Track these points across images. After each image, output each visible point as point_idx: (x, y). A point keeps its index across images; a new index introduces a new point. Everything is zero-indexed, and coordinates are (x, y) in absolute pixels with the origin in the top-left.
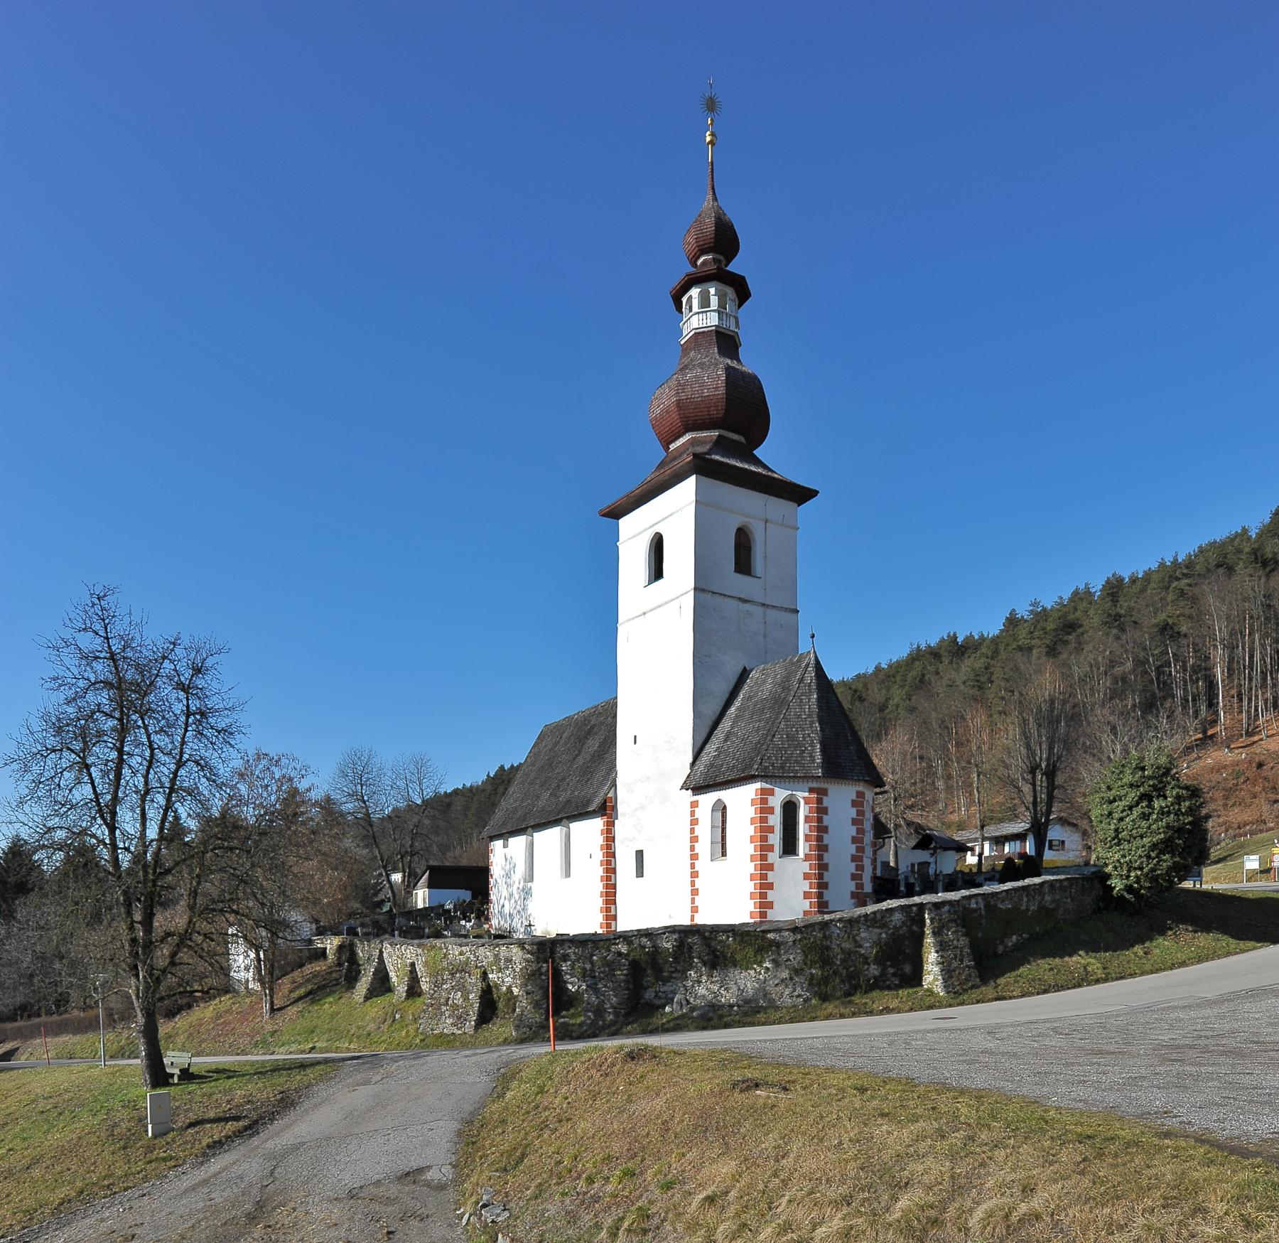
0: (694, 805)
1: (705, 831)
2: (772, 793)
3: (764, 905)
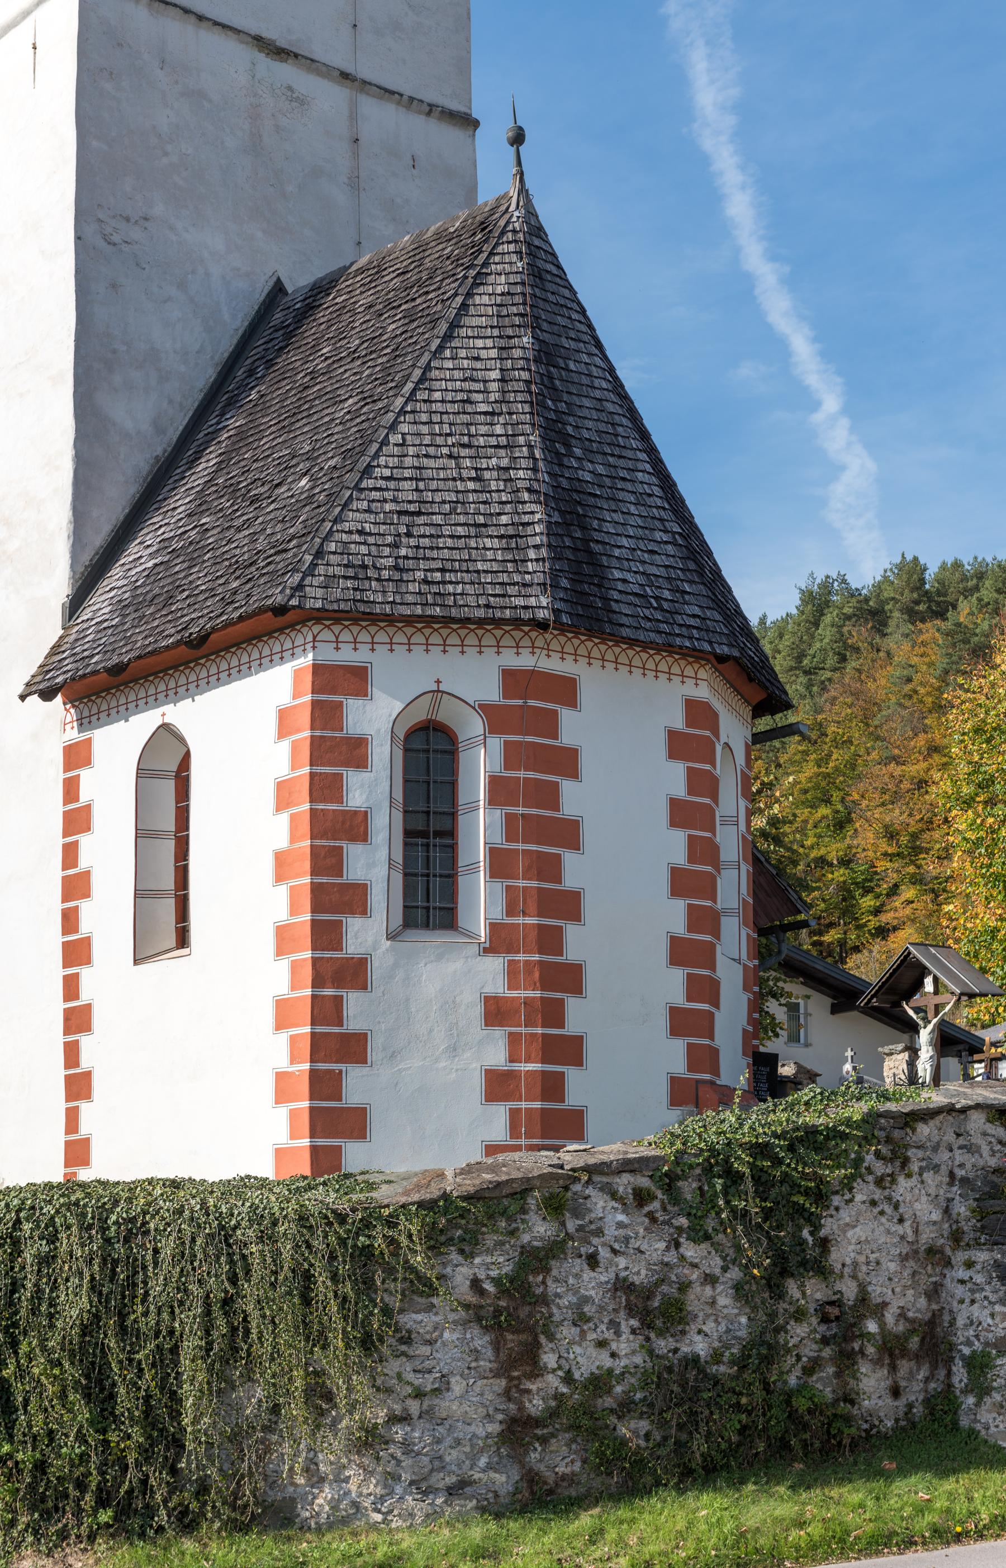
0: (77, 756)
1: (111, 852)
2: (357, 680)
3: (332, 1118)
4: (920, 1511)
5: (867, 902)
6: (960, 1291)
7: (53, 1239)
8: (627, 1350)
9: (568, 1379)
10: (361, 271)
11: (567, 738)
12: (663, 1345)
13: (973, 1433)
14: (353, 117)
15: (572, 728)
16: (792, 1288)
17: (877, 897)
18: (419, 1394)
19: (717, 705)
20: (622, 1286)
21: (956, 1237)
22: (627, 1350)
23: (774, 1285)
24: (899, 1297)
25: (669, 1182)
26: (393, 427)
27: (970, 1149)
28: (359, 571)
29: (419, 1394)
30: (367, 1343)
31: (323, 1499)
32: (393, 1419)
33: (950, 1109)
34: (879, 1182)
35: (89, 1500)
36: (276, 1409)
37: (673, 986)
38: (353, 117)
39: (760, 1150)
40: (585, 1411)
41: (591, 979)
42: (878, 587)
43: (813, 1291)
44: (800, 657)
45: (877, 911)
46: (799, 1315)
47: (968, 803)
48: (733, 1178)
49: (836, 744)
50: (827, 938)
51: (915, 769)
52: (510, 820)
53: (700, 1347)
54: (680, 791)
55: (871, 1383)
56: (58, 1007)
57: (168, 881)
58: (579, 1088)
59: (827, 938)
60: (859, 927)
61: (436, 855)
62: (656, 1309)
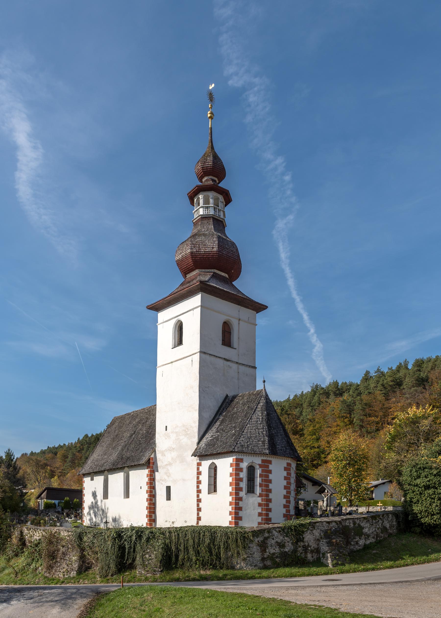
0: (199, 464)
1: (205, 478)
2: (242, 460)
4: (314, 571)
5: (323, 456)
6: (321, 545)
7: (204, 533)
8: (277, 550)
9: (270, 553)
10: (240, 396)
11: (270, 468)
12: (282, 550)
13: (322, 563)
14: (238, 368)
15: (271, 467)
16: (299, 543)
17: (325, 455)
18: (251, 554)
19: (291, 463)
20: (277, 542)
21: (321, 538)
22: (277, 550)
23: (296, 543)
24: (313, 545)
25: (283, 530)
26: (247, 425)
27: (324, 527)
28: (242, 446)
29: (251, 554)
30: (245, 548)
31: (238, 566)
32: (247, 557)
33: (321, 522)
34: (311, 531)
35: (209, 565)
36: (233, 555)
37: (284, 501)
38: (238, 368)
39: (295, 526)
40: (272, 557)
41: (273, 501)
42: (328, 387)
43: (302, 544)
44: (310, 403)
45: (325, 458)
46: (300, 547)
47: (334, 461)
48: (292, 530)
49: (317, 423)
50: (314, 463)
51: (334, 429)
52: (262, 480)
53: (287, 550)
54: (286, 475)
55: (309, 556)
56: (196, 499)
57: (213, 483)
58: (271, 515)
59: (314, 463)
60: (321, 461)
61: (252, 483)
62: (281, 545)
